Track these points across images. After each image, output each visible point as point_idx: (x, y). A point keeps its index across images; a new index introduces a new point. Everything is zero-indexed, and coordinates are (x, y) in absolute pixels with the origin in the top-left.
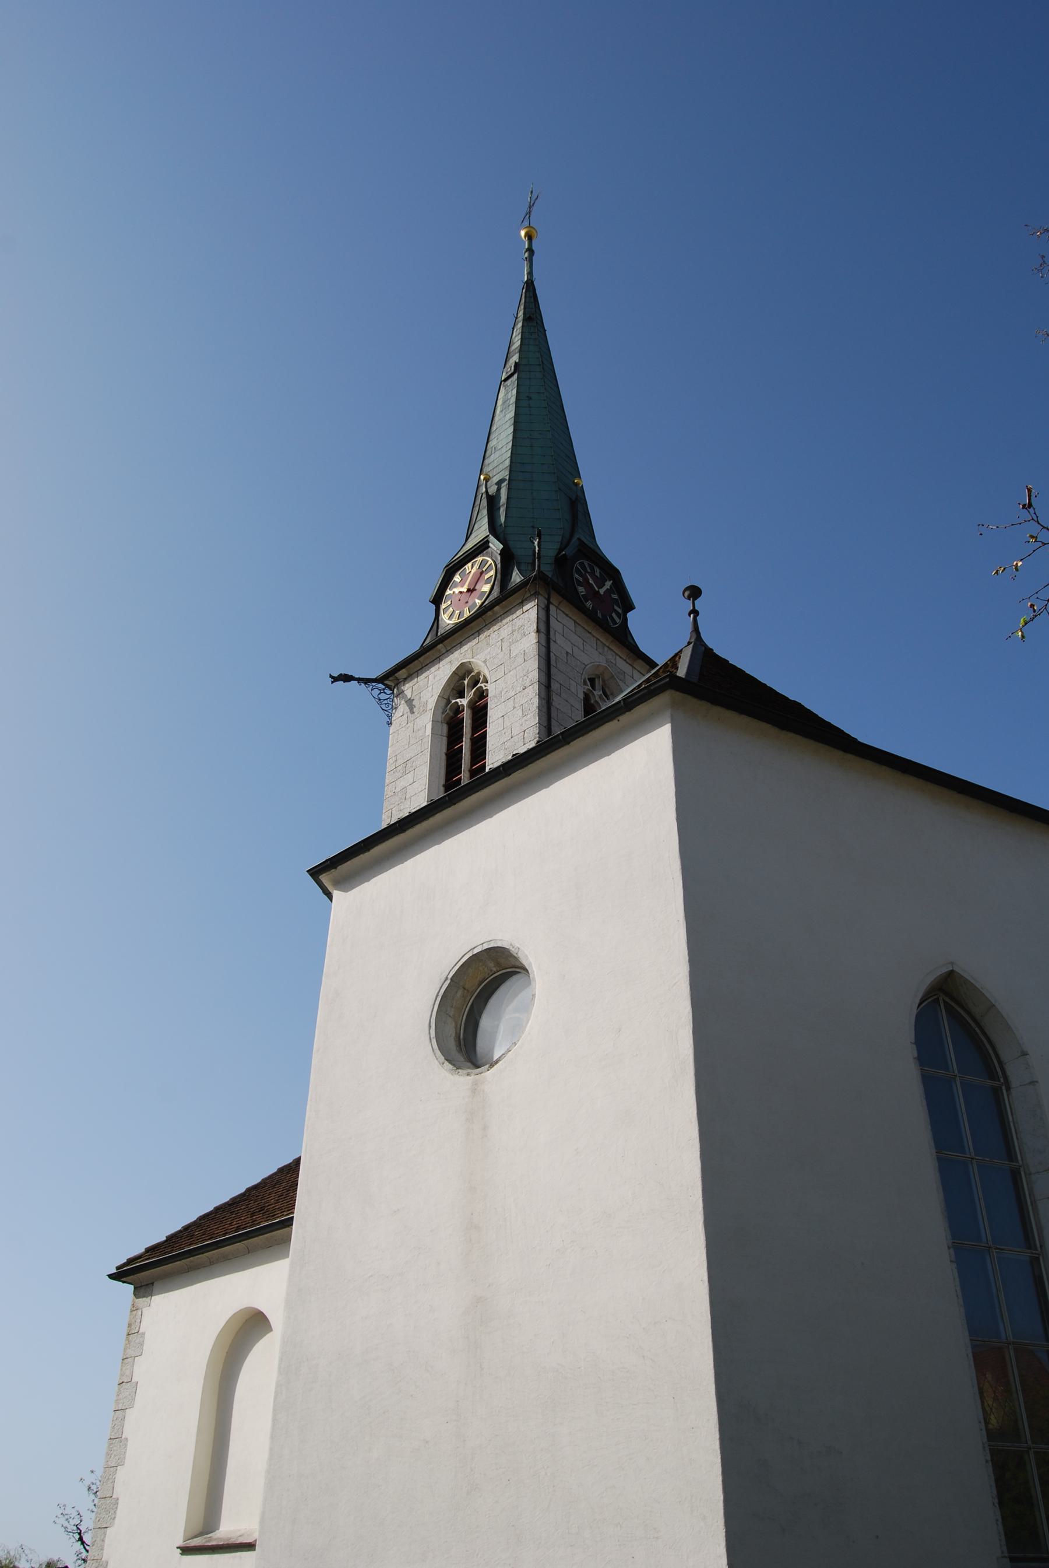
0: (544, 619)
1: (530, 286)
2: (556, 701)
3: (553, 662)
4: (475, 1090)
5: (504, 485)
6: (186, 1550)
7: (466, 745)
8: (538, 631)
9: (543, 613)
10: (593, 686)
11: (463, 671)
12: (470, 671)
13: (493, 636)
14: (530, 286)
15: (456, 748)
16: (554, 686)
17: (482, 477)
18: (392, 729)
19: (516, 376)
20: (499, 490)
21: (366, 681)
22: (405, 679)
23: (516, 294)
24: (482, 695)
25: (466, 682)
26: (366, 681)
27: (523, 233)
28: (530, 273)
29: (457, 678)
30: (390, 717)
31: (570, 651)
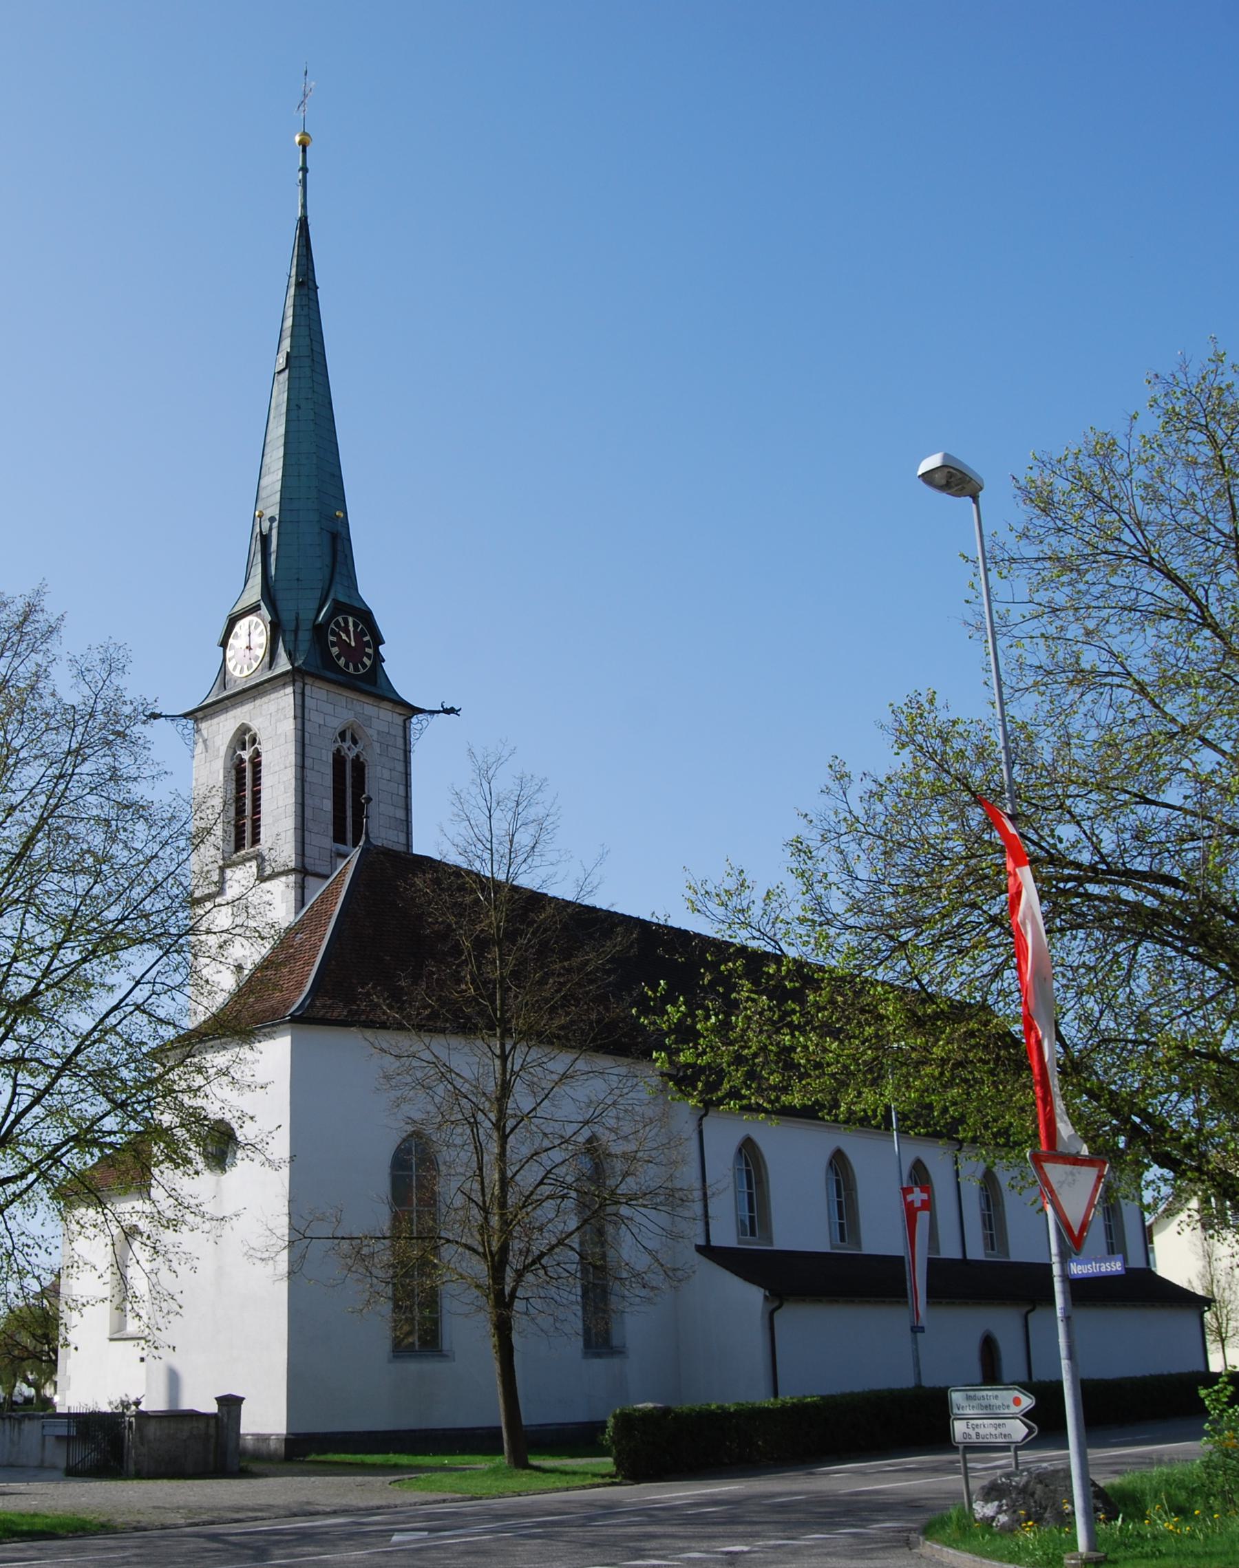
0: (300, 703)
1: (303, 225)
2: (309, 774)
3: (307, 741)
4: (218, 1183)
5: (275, 524)
6: (111, 1340)
7: (248, 793)
8: (295, 718)
9: (299, 697)
10: (343, 740)
11: (243, 729)
12: (249, 729)
13: (265, 706)
14: (303, 225)
15: (273, 573)
16: (308, 763)
17: (257, 513)
18: (195, 763)
19: (287, 371)
20: (271, 529)
21: (173, 717)
22: (202, 719)
23: (292, 233)
24: (257, 754)
25: (247, 738)
26: (173, 717)
27: (297, 139)
28: (304, 206)
29: (240, 732)
30: (192, 751)
31: (322, 723)
